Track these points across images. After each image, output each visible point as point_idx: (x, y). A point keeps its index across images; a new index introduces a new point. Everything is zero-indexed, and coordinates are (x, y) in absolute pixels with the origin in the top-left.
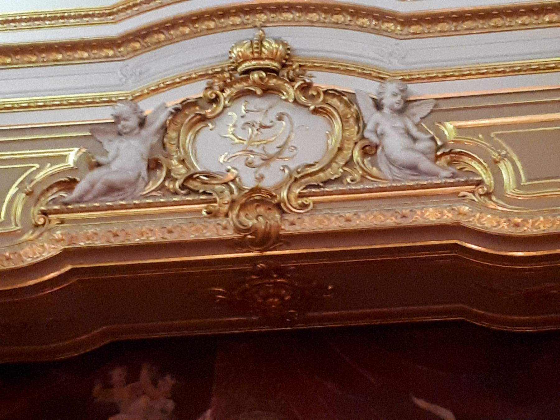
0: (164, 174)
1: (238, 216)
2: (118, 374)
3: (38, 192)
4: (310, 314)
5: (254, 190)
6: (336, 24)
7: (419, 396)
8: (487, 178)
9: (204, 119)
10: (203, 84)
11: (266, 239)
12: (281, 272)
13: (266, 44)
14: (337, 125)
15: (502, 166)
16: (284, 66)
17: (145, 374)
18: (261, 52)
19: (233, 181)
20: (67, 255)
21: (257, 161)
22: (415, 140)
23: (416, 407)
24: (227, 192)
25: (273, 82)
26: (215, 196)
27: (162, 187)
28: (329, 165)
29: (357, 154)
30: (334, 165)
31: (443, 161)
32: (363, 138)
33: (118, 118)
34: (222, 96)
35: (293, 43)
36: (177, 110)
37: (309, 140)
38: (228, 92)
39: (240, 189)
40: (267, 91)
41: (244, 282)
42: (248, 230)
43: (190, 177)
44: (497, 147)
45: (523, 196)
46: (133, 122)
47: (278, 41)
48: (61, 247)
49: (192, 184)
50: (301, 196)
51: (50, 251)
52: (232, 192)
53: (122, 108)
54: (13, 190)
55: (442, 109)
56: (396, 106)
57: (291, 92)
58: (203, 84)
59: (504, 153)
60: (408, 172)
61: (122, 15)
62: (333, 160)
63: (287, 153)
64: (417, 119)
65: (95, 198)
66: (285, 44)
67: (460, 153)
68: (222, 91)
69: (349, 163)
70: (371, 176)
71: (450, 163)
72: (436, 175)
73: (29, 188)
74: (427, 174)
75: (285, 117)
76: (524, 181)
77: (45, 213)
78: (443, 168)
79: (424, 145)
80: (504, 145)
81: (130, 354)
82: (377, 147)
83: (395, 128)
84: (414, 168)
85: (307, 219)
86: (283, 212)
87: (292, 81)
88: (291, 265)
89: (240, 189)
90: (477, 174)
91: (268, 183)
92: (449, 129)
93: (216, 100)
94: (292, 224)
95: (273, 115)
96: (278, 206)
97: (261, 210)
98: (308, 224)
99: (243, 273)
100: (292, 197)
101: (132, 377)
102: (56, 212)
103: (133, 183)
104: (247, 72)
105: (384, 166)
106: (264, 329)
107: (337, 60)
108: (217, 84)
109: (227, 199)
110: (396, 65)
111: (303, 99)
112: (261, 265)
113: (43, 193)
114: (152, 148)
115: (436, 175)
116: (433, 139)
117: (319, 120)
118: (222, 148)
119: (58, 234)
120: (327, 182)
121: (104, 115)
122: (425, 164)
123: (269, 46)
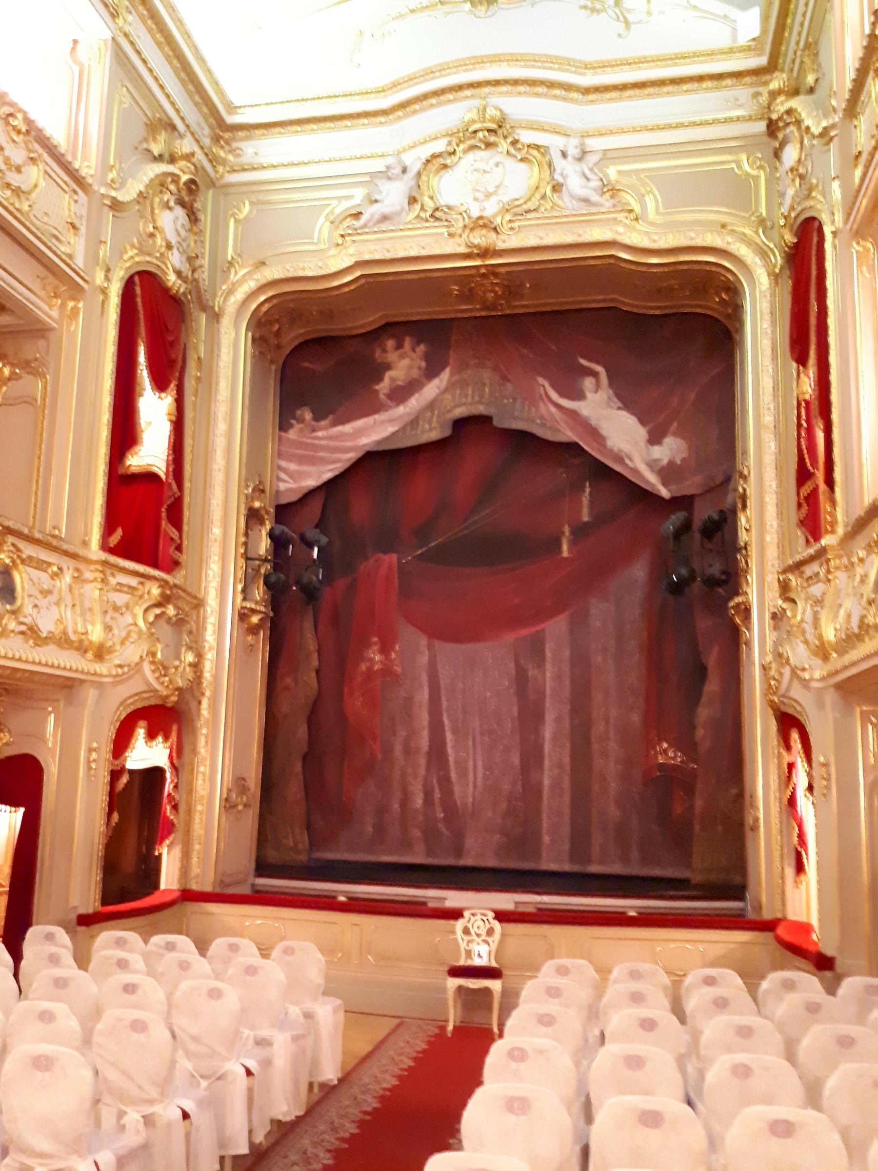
0: (419, 206)
1: (468, 237)
2: (390, 343)
4: (514, 304)
6: (537, 95)
7: (585, 358)
8: (637, 208)
9: (445, 166)
10: (445, 141)
11: (485, 253)
13: (488, 110)
14: (536, 169)
15: (647, 198)
16: (500, 127)
18: (484, 118)
19: (465, 212)
20: (359, 264)
21: (481, 196)
22: (588, 179)
23: (582, 365)
24: (461, 220)
25: (492, 139)
26: (453, 223)
27: (418, 216)
28: (529, 199)
29: (549, 192)
30: (533, 199)
31: (607, 195)
32: (553, 179)
33: (388, 168)
35: (507, 110)
36: (428, 161)
37: (515, 180)
38: (462, 146)
39: (469, 217)
40: (489, 145)
42: (475, 246)
43: (437, 209)
44: (644, 184)
45: (659, 220)
46: (398, 170)
47: (496, 108)
50: (510, 221)
52: (464, 219)
53: (390, 160)
55: (608, 156)
56: (577, 156)
57: (504, 145)
58: (445, 141)
59: (649, 189)
60: (583, 204)
61: (405, 85)
62: (533, 195)
63: (501, 191)
64: (591, 165)
66: (501, 111)
67: (619, 190)
68: (458, 145)
69: (544, 197)
70: (559, 207)
71: (612, 197)
72: (602, 205)
73: (332, 218)
74: (595, 204)
75: (501, 165)
76: (661, 209)
77: (342, 236)
78: (607, 200)
79: (595, 183)
80: (649, 182)
81: (394, 329)
82: (562, 185)
83: (576, 172)
84: (586, 201)
85: (514, 238)
86: (498, 233)
87: (505, 137)
88: (502, 270)
89: (469, 217)
90: (629, 204)
91: (488, 213)
94: (504, 241)
96: (495, 229)
97: (484, 232)
98: (514, 242)
100: (504, 223)
101: (399, 346)
102: (350, 235)
103: (398, 214)
104: (475, 132)
105: (566, 199)
106: (484, 314)
107: (537, 121)
108: (455, 141)
109: (461, 224)
110: (577, 125)
111: (512, 151)
112: (483, 271)
113: (341, 222)
114: (411, 189)
115: (602, 205)
116: (601, 180)
117: (523, 166)
118: (455, 188)
119: (351, 250)
121: (378, 165)
122: (595, 198)
123: (491, 112)
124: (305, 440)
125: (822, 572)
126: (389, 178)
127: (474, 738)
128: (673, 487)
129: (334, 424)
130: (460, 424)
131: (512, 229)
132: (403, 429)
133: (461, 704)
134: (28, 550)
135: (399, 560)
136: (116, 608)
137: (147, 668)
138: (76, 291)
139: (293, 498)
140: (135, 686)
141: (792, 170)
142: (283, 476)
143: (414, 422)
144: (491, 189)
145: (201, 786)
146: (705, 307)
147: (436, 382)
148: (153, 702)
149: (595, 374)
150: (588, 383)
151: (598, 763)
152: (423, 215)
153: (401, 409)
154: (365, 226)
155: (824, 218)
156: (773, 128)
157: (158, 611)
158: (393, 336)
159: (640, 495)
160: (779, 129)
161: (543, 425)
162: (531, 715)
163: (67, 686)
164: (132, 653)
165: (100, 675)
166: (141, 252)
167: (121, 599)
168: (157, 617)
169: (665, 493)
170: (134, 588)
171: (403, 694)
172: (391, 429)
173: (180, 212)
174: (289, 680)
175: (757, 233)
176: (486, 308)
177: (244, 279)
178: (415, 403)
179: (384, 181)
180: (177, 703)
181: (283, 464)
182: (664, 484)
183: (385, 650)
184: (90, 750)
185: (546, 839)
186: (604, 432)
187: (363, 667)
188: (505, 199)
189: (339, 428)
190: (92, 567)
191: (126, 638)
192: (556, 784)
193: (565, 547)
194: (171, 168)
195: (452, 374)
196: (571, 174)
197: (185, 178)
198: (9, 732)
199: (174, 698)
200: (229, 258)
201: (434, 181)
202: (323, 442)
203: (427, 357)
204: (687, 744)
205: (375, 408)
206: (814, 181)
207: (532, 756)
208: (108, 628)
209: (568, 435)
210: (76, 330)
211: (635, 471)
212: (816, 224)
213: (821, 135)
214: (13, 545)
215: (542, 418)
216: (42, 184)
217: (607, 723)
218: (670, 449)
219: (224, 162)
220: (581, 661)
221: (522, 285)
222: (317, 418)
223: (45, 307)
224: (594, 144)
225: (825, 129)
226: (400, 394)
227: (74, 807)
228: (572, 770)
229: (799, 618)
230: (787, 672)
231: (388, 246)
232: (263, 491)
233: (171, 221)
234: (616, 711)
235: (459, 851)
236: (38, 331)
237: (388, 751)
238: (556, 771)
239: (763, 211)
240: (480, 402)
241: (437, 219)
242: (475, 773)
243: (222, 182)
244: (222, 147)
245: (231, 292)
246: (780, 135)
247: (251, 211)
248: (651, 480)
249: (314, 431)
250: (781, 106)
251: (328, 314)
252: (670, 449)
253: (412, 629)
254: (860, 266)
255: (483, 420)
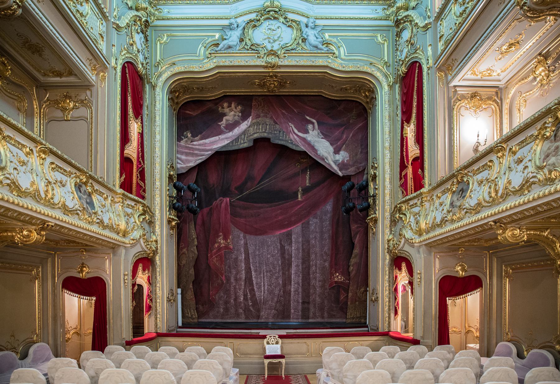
3: (208, 47)
5: (272, 50)
7: (308, 116)
8: (337, 53)
9: (255, 26)
10: (255, 14)
11: (273, 67)
12: (276, 76)
14: (295, 32)
17: (233, 105)
21: (272, 41)
29: (300, 42)
34: (261, 19)
37: (287, 36)
38: (263, 17)
40: (275, 18)
41: (264, 79)
46: (235, 26)
48: (215, 65)
49: (252, 47)
50: (284, 53)
51: (212, 66)
54: (200, 46)
55: (325, 29)
58: (255, 14)
63: (280, 39)
65: (224, 50)
67: (330, 44)
69: (298, 44)
71: (327, 47)
77: (210, 54)
84: (316, 47)
91: (274, 49)
92: (327, 35)
93: (259, 20)
95: (276, 27)
97: (273, 57)
98: (286, 63)
99: (265, 76)
101: (230, 106)
102: (214, 53)
104: (269, 11)
105: (308, 45)
106: (267, 94)
117: (289, 29)
120: (292, 49)
121: (226, 22)
122: (320, 46)
124: (188, 145)
125: (419, 203)
126: (231, 29)
127: (264, 274)
128: (344, 172)
129: (201, 139)
130: (256, 141)
131: (285, 57)
132: (232, 142)
133: (258, 259)
134: (97, 187)
135: (230, 201)
136: (128, 215)
137: (142, 241)
138: (104, 68)
139: (184, 171)
140: (138, 249)
141: (407, 41)
142: (179, 161)
143: (237, 139)
144: (276, 38)
145: (159, 293)
146: (357, 98)
147: (246, 122)
148: (145, 256)
149: (313, 123)
150: (310, 127)
151: (313, 282)
152: (246, 47)
153: (230, 134)
154: (220, 50)
155: (423, 62)
156: (398, 23)
157: (144, 217)
158: (226, 102)
159: (331, 174)
160: (400, 23)
161: (292, 143)
162: (286, 264)
163: (114, 247)
164: (136, 234)
165: (125, 243)
166: (128, 52)
167: (129, 211)
168: (143, 219)
169: (340, 174)
170: (133, 207)
171: (234, 256)
172: (226, 142)
173: (141, 35)
174: (185, 250)
175: (383, 67)
176: (269, 91)
177: (165, 71)
178: (237, 131)
179: (228, 30)
180: (152, 256)
181: (179, 156)
182: (340, 170)
183: (225, 238)
184: (125, 275)
185: (292, 311)
186: (316, 148)
187: (216, 245)
188: (282, 43)
189: (204, 141)
190: (118, 196)
191: (133, 228)
192: (296, 291)
193: (299, 196)
194: (138, 14)
195: (253, 119)
196: (311, 36)
197: (144, 19)
198: (88, 267)
199: (151, 255)
200: (158, 60)
201: (250, 32)
202: (197, 147)
203: (242, 112)
204: (347, 273)
205: (221, 133)
206: (418, 46)
207: (287, 280)
208: (127, 223)
209: (303, 148)
210: (105, 86)
211: (329, 165)
212: (418, 64)
213: (423, 27)
214: (91, 183)
215: (291, 140)
216: (90, 13)
217: (316, 266)
218: (343, 156)
219: (154, 15)
220: (306, 242)
221: (286, 82)
222: (194, 136)
223: (91, 75)
224: (318, 22)
225: (426, 24)
226: (231, 127)
227: (121, 298)
228: (302, 285)
229: (408, 221)
230: (403, 241)
231: (231, 60)
232: (173, 167)
233: (138, 38)
234: (319, 262)
235: (258, 317)
236: (87, 86)
237: (228, 280)
238: (296, 285)
239: (386, 58)
240: (265, 132)
241: (253, 50)
242: (264, 287)
243: (153, 24)
244: (153, 7)
245: (160, 76)
246: (401, 26)
247: (167, 39)
248: (335, 168)
249: (192, 142)
250: (403, 14)
251: (201, 90)
252: (343, 156)
253: (236, 230)
254: (439, 82)
255: (267, 140)
